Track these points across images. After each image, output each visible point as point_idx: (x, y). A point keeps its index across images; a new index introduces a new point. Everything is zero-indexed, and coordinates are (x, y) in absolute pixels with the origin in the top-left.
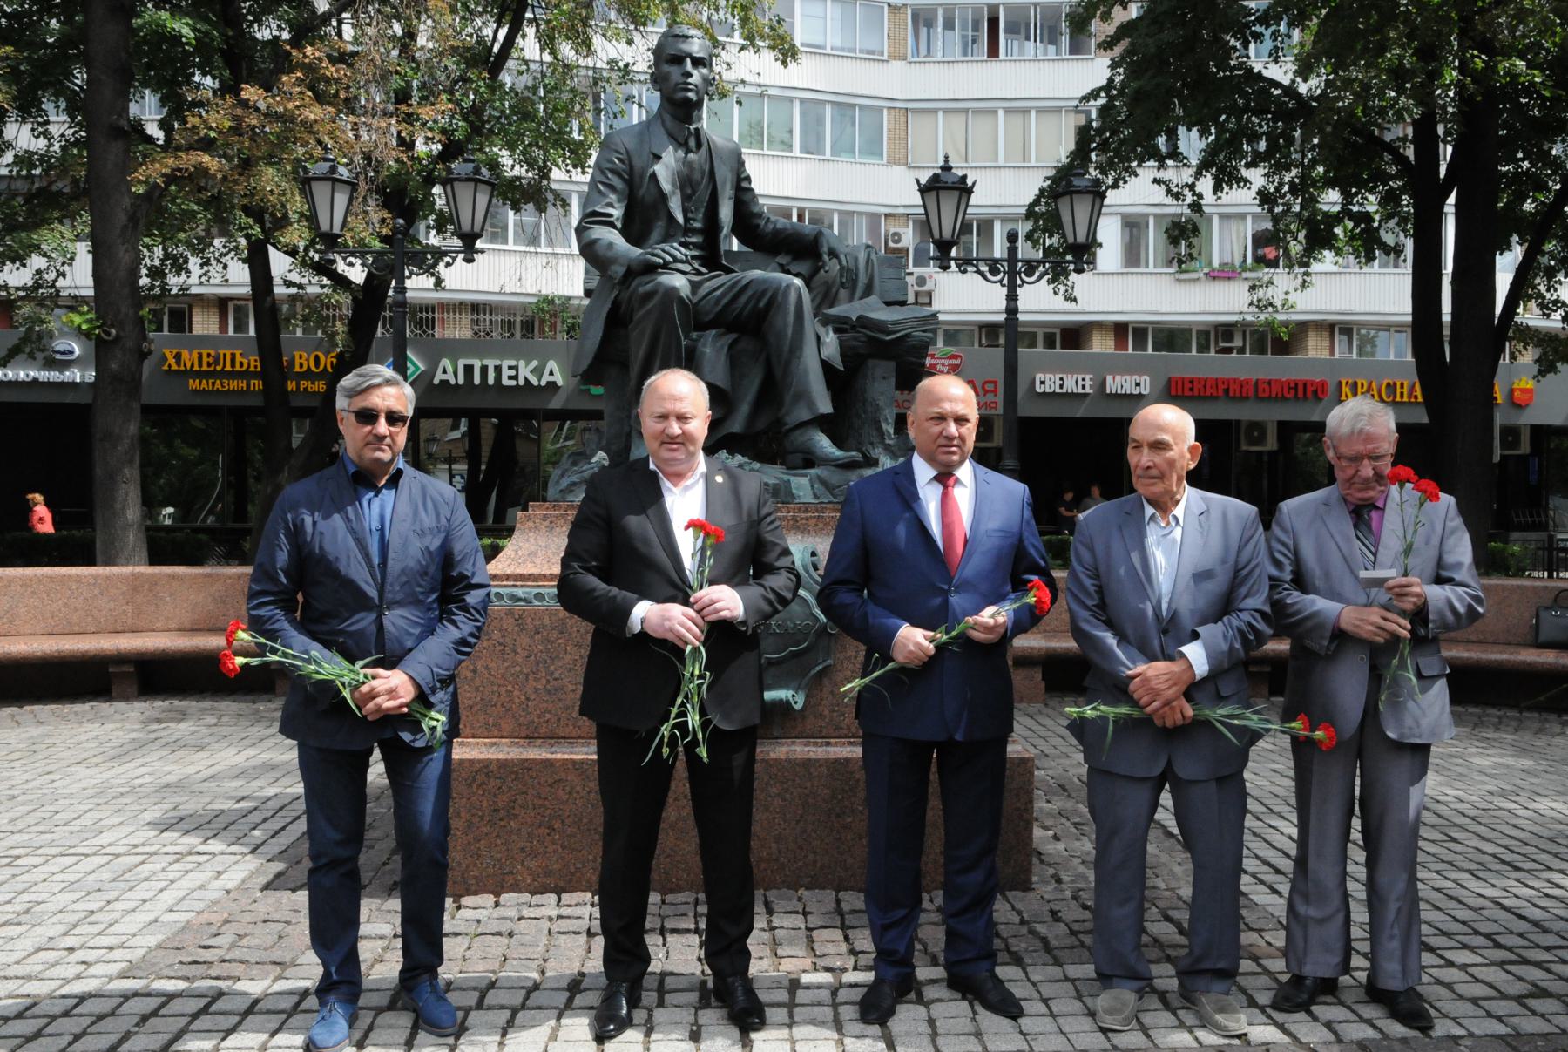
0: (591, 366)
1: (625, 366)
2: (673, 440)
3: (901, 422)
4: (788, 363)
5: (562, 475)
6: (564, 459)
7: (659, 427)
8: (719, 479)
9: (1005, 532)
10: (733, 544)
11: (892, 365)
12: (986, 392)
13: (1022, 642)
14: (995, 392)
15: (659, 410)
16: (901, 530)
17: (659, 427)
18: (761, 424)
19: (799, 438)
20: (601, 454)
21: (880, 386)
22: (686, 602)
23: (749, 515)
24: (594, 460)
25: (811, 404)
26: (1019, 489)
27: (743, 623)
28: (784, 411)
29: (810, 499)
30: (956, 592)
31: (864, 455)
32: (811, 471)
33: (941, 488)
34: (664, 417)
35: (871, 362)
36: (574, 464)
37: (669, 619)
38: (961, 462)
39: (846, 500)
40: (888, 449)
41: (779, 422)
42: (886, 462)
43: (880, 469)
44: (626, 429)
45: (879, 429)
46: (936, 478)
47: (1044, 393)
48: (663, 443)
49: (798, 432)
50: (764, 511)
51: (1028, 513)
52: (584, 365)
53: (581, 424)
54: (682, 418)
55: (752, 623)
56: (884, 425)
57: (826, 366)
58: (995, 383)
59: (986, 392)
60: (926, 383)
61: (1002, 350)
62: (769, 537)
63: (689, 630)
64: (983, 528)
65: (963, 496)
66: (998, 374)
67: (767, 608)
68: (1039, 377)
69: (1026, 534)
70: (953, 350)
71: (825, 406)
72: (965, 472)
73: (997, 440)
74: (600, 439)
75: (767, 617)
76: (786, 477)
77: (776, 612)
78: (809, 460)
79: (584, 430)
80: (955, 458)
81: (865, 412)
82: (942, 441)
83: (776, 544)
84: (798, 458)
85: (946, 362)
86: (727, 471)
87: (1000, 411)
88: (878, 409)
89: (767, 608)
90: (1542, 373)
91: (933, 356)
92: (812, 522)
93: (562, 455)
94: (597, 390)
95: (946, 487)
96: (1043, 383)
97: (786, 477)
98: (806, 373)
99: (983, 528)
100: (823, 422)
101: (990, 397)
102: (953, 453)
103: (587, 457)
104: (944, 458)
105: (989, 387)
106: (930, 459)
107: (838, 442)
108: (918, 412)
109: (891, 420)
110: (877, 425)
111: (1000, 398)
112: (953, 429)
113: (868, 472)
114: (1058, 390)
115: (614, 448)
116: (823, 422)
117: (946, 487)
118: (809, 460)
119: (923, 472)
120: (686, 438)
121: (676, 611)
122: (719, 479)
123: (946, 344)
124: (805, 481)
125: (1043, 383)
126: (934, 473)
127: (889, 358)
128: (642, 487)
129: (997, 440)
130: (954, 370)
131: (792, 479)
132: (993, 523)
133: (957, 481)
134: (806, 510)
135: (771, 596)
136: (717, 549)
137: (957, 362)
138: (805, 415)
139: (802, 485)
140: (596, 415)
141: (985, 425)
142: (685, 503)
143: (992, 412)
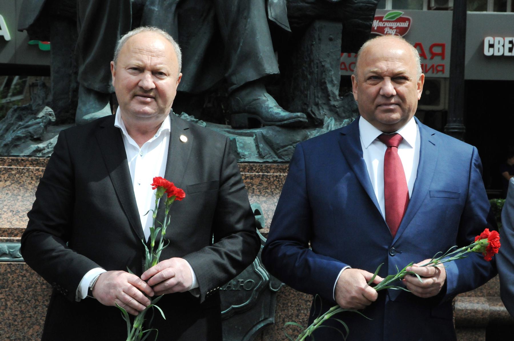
0: (38, 20)
1: (72, 21)
2: (146, 92)
3: (346, 84)
4: (235, 24)
5: (7, 130)
6: (10, 112)
7: (134, 78)
8: (184, 139)
9: (449, 194)
10: (191, 207)
11: (339, 26)
12: (433, 55)
13: (466, 304)
14: (442, 55)
15: (135, 63)
16: (343, 188)
17: (134, 78)
18: (208, 84)
19: (246, 98)
20: (48, 109)
21: (326, 49)
22: (139, 273)
23: (210, 175)
24: (41, 115)
25: (258, 65)
26: (467, 150)
27: (197, 290)
28: (230, 71)
29: (254, 158)
30: (397, 251)
31: (309, 116)
32: (257, 131)
33: (384, 148)
34: (140, 70)
35: (318, 24)
36: (20, 118)
37: (115, 286)
38: (404, 120)
39: (293, 159)
40: (333, 110)
41: (226, 82)
42: (332, 124)
43: (324, 131)
44: (73, 85)
45: (325, 90)
46: (380, 139)
47: (493, 57)
48: (135, 96)
49: (243, 93)
50: (228, 172)
51: (475, 175)
52: (30, 20)
53: (30, 80)
54: (157, 73)
55: (205, 291)
56: (329, 87)
57: (273, 26)
58: (443, 46)
59: (433, 55)
60: (368, 44)
61: (450, 13)
62: (231, 198)
63: (134, 297)
64: (425, 189)
65: (408, 158)
66: (445, 36)
67: (221, 275)
68: (489, 40)
69: (473, 196)
70: (401, 13)
71: (271, 67)
72: (411, 131)
73: (443, 104)
74: (47, 95)
75: (221, 283)
76: (231, 137)
77: (231, 276)
78: (255, 120)
79: (33, 86)
80: (396, 116)
81: (311, 73)
82: (380, 100)
83: (238, 207)
84: (243, 118)
85: (394, 25)
86: (193, 131)
87: (447, 74)
88: (324, 70)
89: (221, 275)
90: (406, 79)
91: (380, 19)
92: (257, 181)
93: (7, 109)
94: (45, 46)
95: (390, 146)
96: (491, 46)
97: (231, 137)
98: (253, 34)
99: (425, 189)
100: (268, 83)
101: (437, 60)
102: (392, 111)
103: (34, 113)
104: (384, 116)
105: (437, 50)
106: (373, 120)
107: (283, 102)
108: (361, 71)
109: (337, 82)
110: (322, 86)
111: (447, 62)
112: (390, 87)
113: (314, 133)
114: (507, 54)
115: (61, 104)
116: (268, 83)
117: (390, 146)
118: (255, 120)
119: (368, 132)
120: (157, 94)
121: (124, 279)
122: (184, 139)
123: (394, 7)
124: (250, 141)
125: (491, 46)
126: (379, 133)
127: (335, 20)
128: (108, 149)
129: (443, 104)
130: (402, 32)
131: (239, 138)
132: (436, 184)
133: (402, 141)
134: (251, 169)
135: (225, 262)
136: (174, 209)
137: (405, 25)
138: (251, 75)
139: (247, 145)
140: (43, 71)
141: (430, 87)
142: (147, 164)
143: (440, 75)
